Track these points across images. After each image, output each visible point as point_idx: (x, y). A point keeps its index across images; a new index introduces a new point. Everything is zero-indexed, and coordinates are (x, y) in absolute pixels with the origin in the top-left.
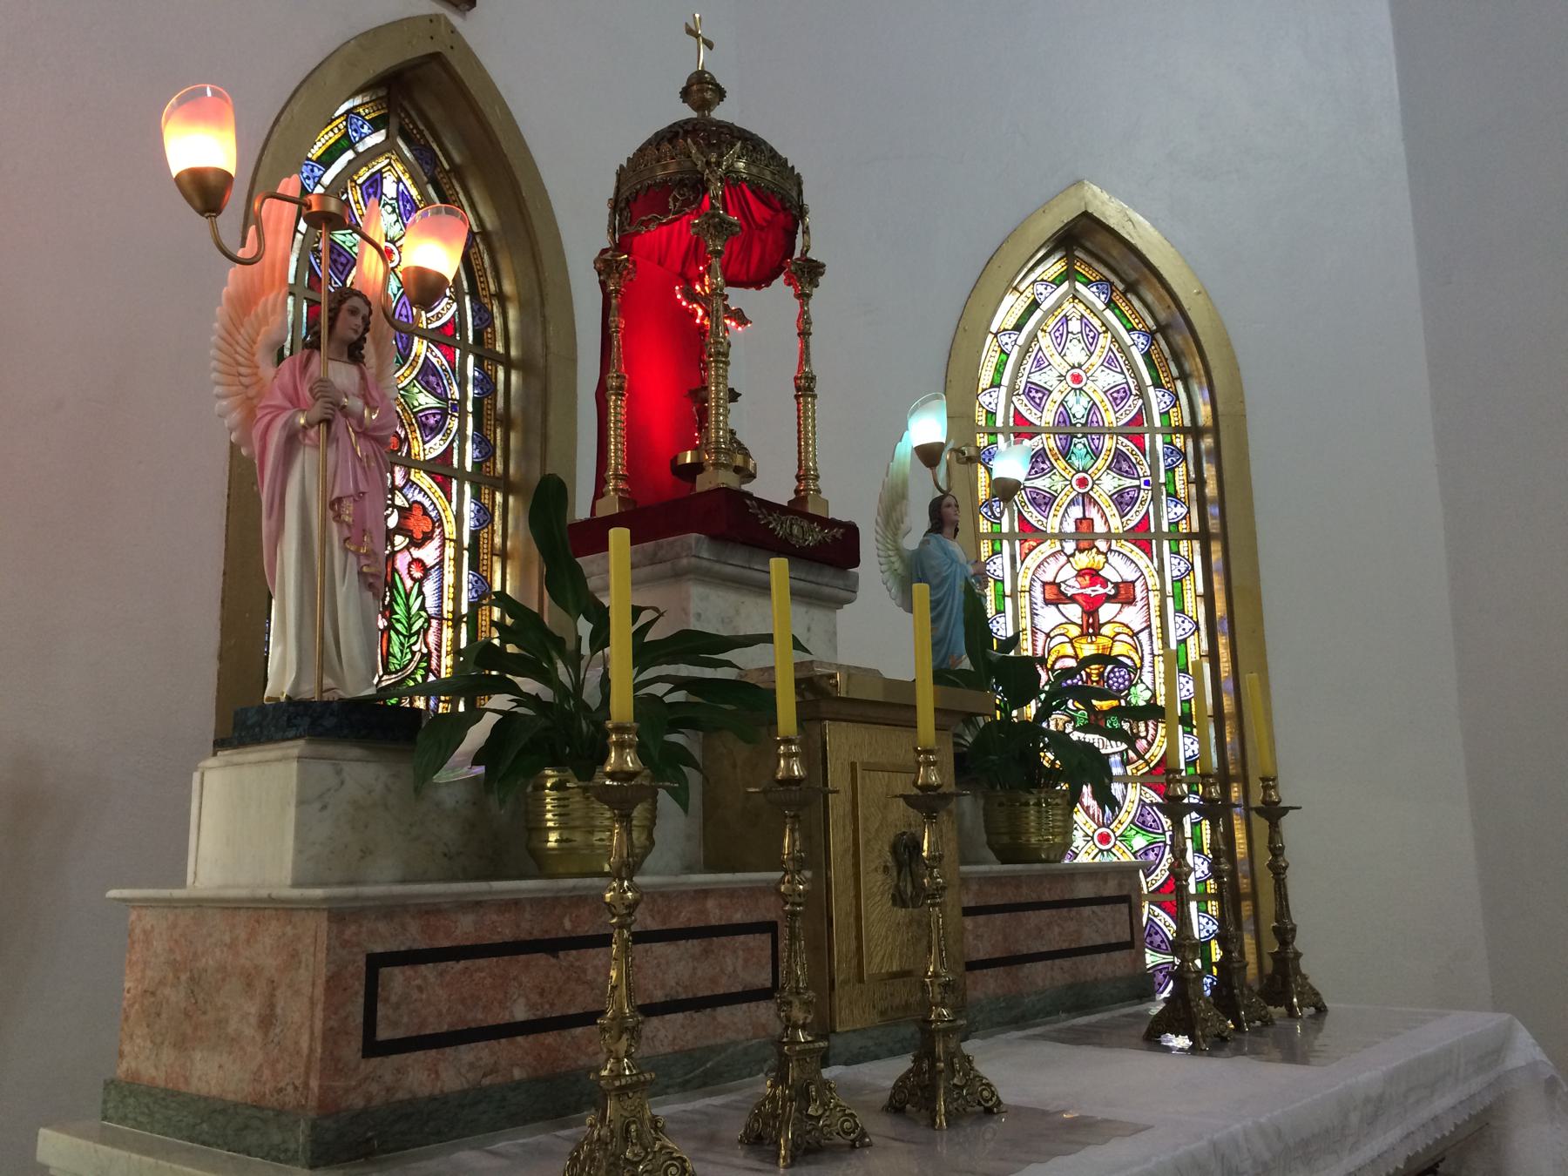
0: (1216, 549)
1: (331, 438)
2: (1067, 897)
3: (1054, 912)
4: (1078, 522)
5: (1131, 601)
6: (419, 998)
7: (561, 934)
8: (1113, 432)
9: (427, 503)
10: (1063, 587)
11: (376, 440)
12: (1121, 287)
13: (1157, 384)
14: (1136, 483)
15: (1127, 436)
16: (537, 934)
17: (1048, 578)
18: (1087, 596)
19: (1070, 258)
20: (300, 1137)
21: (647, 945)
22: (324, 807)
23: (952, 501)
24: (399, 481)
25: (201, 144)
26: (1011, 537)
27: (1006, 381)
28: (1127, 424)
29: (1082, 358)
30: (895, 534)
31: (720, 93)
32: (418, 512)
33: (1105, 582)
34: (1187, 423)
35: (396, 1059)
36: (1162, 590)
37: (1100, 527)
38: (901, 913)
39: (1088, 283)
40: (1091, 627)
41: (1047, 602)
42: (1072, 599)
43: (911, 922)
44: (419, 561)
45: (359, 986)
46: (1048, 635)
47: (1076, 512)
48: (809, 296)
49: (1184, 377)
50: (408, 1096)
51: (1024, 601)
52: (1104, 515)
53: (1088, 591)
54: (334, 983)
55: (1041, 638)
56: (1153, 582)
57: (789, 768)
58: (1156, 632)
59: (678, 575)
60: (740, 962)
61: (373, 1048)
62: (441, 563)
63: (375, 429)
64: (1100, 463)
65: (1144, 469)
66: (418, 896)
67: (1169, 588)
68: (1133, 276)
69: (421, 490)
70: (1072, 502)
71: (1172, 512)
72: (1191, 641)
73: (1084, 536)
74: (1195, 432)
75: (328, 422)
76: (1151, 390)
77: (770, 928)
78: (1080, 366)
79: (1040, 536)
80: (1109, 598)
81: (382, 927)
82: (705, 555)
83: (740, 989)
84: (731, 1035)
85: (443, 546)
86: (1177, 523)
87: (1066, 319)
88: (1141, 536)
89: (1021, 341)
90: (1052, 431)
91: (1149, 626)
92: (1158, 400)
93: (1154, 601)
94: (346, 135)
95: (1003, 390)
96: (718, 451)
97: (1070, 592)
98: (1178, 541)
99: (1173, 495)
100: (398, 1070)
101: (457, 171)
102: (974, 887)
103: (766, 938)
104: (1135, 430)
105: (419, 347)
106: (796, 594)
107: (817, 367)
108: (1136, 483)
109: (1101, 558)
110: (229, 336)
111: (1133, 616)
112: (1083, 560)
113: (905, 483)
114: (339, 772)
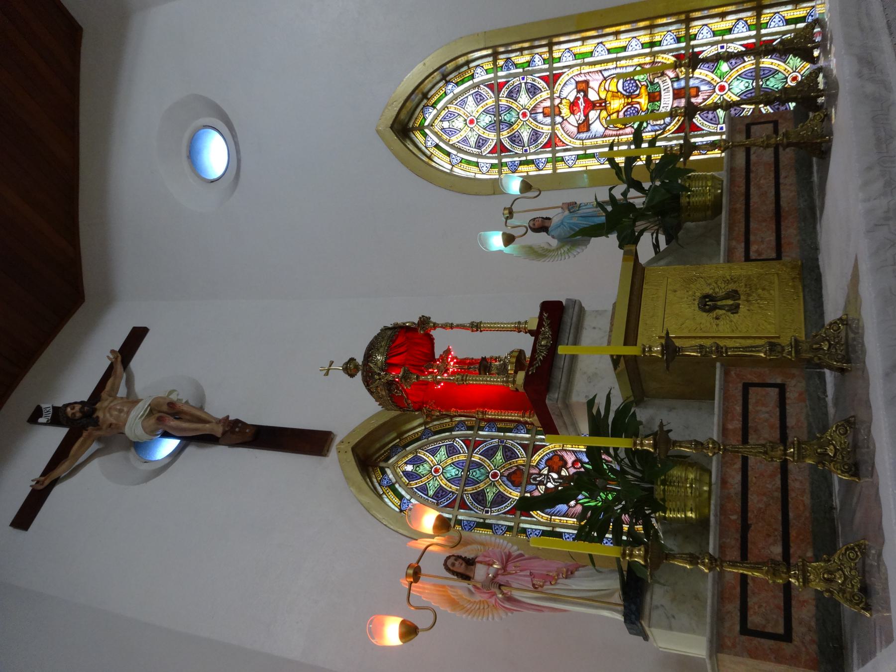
0: (556, 40)
1: (508, 585)
2: (744, 174)
3: (752, 183)
4: (545, 115)
5: (587, 82)
6: (764, 611)
7: (739, 522)
8: (498, 100)
9: (546, 458)
10: (580, 122)
11: (507, 561)
12: (425, 101)
13: (472, 77)
14: (523, 85)
15: (499, 91)
16: (738, 536)
17: (575, 130)
18: (585, 107)
19: (414, 129)
21: (749, 468)
22: (674, 617)
23: (532, 223)
24: (535, 471)
25: (391, 632)
26: (554, 152)
27: (474, 159)
28: (493, 92)
29: (461, 119)
30: (550, 251)
31: (352, 360)
32: (550, 463)
33: (577, 99)
34: (491, 59)
35: (795, 624)
36: (580, 65)
37: (547, 103)
38: (743, 309)
40: (602, 105)
41: (588, 130)
42: (586, 116)
43: (748, 301)
44: (574, 463)
45: (756, 641)
46: (606, 129)
47: (540, 117)
48: (434, 324)
49: (467, 63)
50: (814, 619)
51: (588, 143)
52: (541, 102)
53: (582, 107)
55: (608, 132)
56: (576, 71)
57: (649, 445)
58: (603, 67)
59: (567, 406)
60: (764, 409)
61: (787, 637)
63: (502, 563)
64: (514, 106)
66: (713, 603)
68: (420, 96)
69: (540, 460)
70: (535, 120)
71: (539, 64)
72: (609, 46)
73: (553, 112)
74: (495, 55)
75: (500, 585)
76: (475, 81)
77: (746, 387)
78: (465, 120)
79: (553, 135)
80: (586, 95)
81: (727, 624)
82: (556, 396)
83: (778, 409)
85: (566, 450)
86: (544, 60)
87: (443, 129)
88: (551, 81)
90: (499, 132)
91: (601, 71)
92: (481, 76)
93: (586, 69)
94: (389, 487)
95: (480, 160)
96: (507, 382)
97: (583, 118)
98: (553, 58)
99: (529, 63)
100: (800, 623)
101: (400, 435)
102: (734, 243)
103: (752, 390)
104: (496, 87)
105: (476, 458)
106: (576, 342)
107: (467, 321)
108: (523, 85)
109: (564, 101)
110: (468, 611)
111: (594, 84)
112: (565, 111)
113: (524, 247)
114: (657, 607)
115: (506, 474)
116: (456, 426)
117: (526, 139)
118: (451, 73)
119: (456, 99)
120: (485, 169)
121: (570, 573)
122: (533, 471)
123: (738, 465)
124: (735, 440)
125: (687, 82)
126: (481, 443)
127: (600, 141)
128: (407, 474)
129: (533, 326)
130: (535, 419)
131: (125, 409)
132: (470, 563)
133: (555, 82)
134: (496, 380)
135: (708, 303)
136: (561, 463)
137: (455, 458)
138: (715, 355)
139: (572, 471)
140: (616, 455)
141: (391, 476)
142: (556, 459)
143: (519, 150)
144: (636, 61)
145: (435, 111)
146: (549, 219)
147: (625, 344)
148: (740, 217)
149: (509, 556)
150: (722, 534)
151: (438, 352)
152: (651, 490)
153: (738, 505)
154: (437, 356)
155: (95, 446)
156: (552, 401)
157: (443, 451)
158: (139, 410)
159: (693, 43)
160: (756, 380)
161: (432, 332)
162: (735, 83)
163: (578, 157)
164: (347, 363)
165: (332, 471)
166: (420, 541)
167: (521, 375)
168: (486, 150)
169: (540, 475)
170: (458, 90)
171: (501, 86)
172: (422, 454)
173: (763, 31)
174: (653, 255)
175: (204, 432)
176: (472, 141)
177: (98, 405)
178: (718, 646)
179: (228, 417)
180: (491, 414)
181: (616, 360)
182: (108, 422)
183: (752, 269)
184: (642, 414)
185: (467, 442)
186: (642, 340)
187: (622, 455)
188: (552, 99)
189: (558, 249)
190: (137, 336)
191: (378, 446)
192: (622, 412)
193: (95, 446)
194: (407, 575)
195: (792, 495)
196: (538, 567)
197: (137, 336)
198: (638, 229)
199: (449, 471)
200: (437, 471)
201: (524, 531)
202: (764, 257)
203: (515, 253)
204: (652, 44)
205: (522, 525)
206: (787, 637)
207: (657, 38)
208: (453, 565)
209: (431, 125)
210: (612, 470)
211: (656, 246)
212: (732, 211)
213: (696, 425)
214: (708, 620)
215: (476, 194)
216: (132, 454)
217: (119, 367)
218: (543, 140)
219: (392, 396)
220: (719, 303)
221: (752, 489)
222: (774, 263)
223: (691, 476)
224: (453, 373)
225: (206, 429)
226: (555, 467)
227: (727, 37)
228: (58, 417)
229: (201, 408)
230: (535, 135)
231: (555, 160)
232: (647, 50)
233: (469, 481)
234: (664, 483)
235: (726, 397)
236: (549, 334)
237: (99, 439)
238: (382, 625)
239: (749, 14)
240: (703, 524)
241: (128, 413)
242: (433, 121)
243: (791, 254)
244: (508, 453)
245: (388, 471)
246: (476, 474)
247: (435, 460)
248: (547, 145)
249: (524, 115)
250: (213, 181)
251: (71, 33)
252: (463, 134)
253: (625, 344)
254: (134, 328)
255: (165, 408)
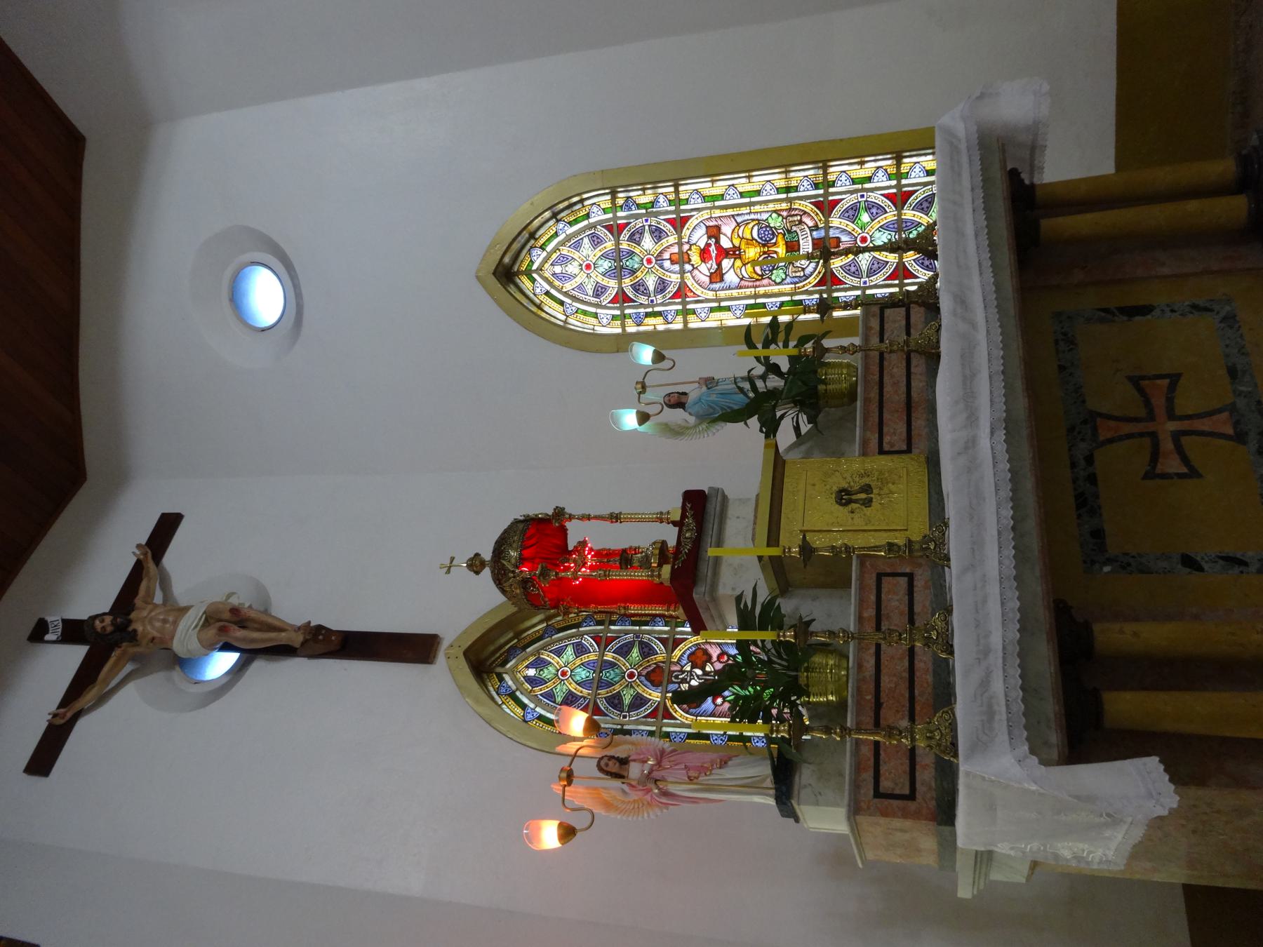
1: (663, 780)
4: (673, 262)
5: (718, 228)
6: (894, 778)
8: (618, 243)
12: (532, 242)
13: (588, 216)
16: (872, 714)
17: (707, 280)
19: (519, 273)
20: (947, 829)
24: (678, 668)
25: (549, 835)
26: (684, 303)
27: (592, 310)
29: (576, 264)
30: (688, 428)
31: (477, 555)
32: (693, 658)
33: (708, 245)
34: (609, 197)
35: (918, 786)
37: (675, 249)
38: (875, 504)
39: (532, 262)
40: (735, 253)
41: (722, 280)
42: (719, 265)
44: (719, 657)
45: (886, 802)
47: (667, 264)
49: (582, 201)
51: (722, 294)
53: (714, 255)
54: (885, 814)
56: (705, 214)
59: (714, 599)
60: (896, 598)
61: (912, 796)
62: (719, 645)
64: (637, 251)
65: (639, 223)
67: (709, 205)
70: (662, 267)
74: (614, 194)
76: (591, 220)
77: (880, 576)
84: (927, 603)
89: (569, 301)
90: (620, 279)
93: (717, 213)
95: (599, 311)
96: (652, 576)
97: (715, 266)
99: (653, 204)
101: (517, 635)
102: (868, 434)
103: (885, 579)
104: (615, 229)
105: (609, 656)
107: (606, 512)
111: (727, 229)
112: (695, 258)
115: (644, 673)
116: (584, 621)
117: (651, 288)
118: (562, 210)
119: (569, 240)
120: (605, 321)
121: (723, 763)
122: (674, 668)
123: (873, 650)
124: (869, 628)
125: (827, 232)
126: (614, 639)
127: (735, 293)
128: (529, 680)
129: (677, 516)
130: (680, 612)
131: (171, 619)
132: (624, 762)
133: (683, 227)
134: (641, 575)
135: (844, 497)
136: (705, 658)
137: (585, 658)
138: (842, 556)
139: (719, 666)
140: (764, 646)
141: (510, 683)
142: (700, 654)
143: (643, 300)
144: (771, 207)
145: (545, 254)
146: (685, 394)
147: (768, 545)
148: (874, 407)
149: (663, 752)
150: (858, 713)
151: (571, 545)
152: (796, 678)
153: (872, 686)
154: (570, 548)
155: (129, 667)
156: (699, 594)
157: (570, 651)
158: (189, 622)
159: (831, 190)
160: (889, 570)
161: (568, 524)
162: (877, 235)
163: (712, 310)
164: (471, 559)
165: (442, 679)
166: (569, 745)
167: (667, 569)
168: (606, 299)
169: (683, 672)
170: (570, 230)
171: (621, 228)
172: (545, 656)
173: (904, 182)
174: (795, 439)
175: (261, 638)
176: (590, 289)
177: (133, 616)
178: (855, 810)
179: (309, 622)
180: (634, 609)
181: (760, 558)
182: (150, 636)
183: (885, 462)
184: (787, 606)
185: (597, 639)
186: (784, 540)
187: (769, 646)
188: (680, 244)
189: (695, 426)
190: (168, 525)
191: (492, 648)
192: (769, 606)
193: (129, 667)
194: (560, 779)
195: (917, 674)
196: (694, 759)
197: (168, 525)
198: (779, 414)
199: (579, 674)
200: (564, 674)
201: (668, 735)
202: (896, 448)
203: (650, 432)
204: (788, 189)
205: (665, 729)
206: (912, 796)
207: (794, 183)
208: (607, 765)
209: (540, 269)
210: (760, 660)
211: (797, 428)
212: (867, 401)
213: (833, 613)
214: (847, 787)
215: (597, 351)
216: (176, 674)
217: (151, 565)
218: (672, 289)
219: (527, 593)
220: (854, 497)
221: (884, 671)
222: (904, 456)
223: (831, 662)
224: (591, 568)
225: (282, 639)
226: (699, 662)
227: (867, 186)
228: (73, 632)
229: (266, 612)
230: (662, 286)
231: (686, 313)
232: (784, 196)
233: (602, 684)
234: (807, 670)
235: (862, 588)
236: (693, 526)
237: (134, 659)
238: (539, 829)
239: (889, 162)
240: (842, 705)
241: (175, 623)
242: (542, 264)
243: (920, 445)
244: (646, 650)
245: (507, 677)
246: (610, 675)
247: (561, 661)
248: (676, 295)
249: (649, 261)
250: (263, 330)
251: (69, 144)
252: (578, 280)
253: (768, 545)
254: (163, 515)
255: (227, 615)
